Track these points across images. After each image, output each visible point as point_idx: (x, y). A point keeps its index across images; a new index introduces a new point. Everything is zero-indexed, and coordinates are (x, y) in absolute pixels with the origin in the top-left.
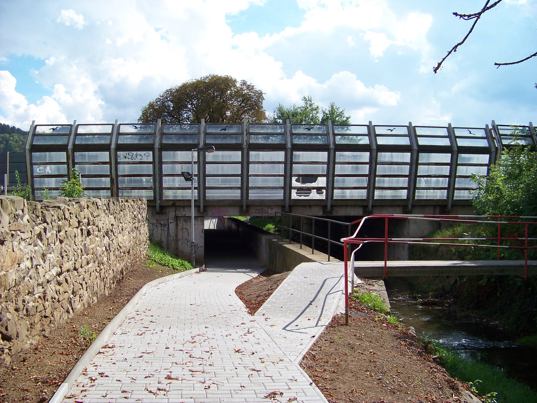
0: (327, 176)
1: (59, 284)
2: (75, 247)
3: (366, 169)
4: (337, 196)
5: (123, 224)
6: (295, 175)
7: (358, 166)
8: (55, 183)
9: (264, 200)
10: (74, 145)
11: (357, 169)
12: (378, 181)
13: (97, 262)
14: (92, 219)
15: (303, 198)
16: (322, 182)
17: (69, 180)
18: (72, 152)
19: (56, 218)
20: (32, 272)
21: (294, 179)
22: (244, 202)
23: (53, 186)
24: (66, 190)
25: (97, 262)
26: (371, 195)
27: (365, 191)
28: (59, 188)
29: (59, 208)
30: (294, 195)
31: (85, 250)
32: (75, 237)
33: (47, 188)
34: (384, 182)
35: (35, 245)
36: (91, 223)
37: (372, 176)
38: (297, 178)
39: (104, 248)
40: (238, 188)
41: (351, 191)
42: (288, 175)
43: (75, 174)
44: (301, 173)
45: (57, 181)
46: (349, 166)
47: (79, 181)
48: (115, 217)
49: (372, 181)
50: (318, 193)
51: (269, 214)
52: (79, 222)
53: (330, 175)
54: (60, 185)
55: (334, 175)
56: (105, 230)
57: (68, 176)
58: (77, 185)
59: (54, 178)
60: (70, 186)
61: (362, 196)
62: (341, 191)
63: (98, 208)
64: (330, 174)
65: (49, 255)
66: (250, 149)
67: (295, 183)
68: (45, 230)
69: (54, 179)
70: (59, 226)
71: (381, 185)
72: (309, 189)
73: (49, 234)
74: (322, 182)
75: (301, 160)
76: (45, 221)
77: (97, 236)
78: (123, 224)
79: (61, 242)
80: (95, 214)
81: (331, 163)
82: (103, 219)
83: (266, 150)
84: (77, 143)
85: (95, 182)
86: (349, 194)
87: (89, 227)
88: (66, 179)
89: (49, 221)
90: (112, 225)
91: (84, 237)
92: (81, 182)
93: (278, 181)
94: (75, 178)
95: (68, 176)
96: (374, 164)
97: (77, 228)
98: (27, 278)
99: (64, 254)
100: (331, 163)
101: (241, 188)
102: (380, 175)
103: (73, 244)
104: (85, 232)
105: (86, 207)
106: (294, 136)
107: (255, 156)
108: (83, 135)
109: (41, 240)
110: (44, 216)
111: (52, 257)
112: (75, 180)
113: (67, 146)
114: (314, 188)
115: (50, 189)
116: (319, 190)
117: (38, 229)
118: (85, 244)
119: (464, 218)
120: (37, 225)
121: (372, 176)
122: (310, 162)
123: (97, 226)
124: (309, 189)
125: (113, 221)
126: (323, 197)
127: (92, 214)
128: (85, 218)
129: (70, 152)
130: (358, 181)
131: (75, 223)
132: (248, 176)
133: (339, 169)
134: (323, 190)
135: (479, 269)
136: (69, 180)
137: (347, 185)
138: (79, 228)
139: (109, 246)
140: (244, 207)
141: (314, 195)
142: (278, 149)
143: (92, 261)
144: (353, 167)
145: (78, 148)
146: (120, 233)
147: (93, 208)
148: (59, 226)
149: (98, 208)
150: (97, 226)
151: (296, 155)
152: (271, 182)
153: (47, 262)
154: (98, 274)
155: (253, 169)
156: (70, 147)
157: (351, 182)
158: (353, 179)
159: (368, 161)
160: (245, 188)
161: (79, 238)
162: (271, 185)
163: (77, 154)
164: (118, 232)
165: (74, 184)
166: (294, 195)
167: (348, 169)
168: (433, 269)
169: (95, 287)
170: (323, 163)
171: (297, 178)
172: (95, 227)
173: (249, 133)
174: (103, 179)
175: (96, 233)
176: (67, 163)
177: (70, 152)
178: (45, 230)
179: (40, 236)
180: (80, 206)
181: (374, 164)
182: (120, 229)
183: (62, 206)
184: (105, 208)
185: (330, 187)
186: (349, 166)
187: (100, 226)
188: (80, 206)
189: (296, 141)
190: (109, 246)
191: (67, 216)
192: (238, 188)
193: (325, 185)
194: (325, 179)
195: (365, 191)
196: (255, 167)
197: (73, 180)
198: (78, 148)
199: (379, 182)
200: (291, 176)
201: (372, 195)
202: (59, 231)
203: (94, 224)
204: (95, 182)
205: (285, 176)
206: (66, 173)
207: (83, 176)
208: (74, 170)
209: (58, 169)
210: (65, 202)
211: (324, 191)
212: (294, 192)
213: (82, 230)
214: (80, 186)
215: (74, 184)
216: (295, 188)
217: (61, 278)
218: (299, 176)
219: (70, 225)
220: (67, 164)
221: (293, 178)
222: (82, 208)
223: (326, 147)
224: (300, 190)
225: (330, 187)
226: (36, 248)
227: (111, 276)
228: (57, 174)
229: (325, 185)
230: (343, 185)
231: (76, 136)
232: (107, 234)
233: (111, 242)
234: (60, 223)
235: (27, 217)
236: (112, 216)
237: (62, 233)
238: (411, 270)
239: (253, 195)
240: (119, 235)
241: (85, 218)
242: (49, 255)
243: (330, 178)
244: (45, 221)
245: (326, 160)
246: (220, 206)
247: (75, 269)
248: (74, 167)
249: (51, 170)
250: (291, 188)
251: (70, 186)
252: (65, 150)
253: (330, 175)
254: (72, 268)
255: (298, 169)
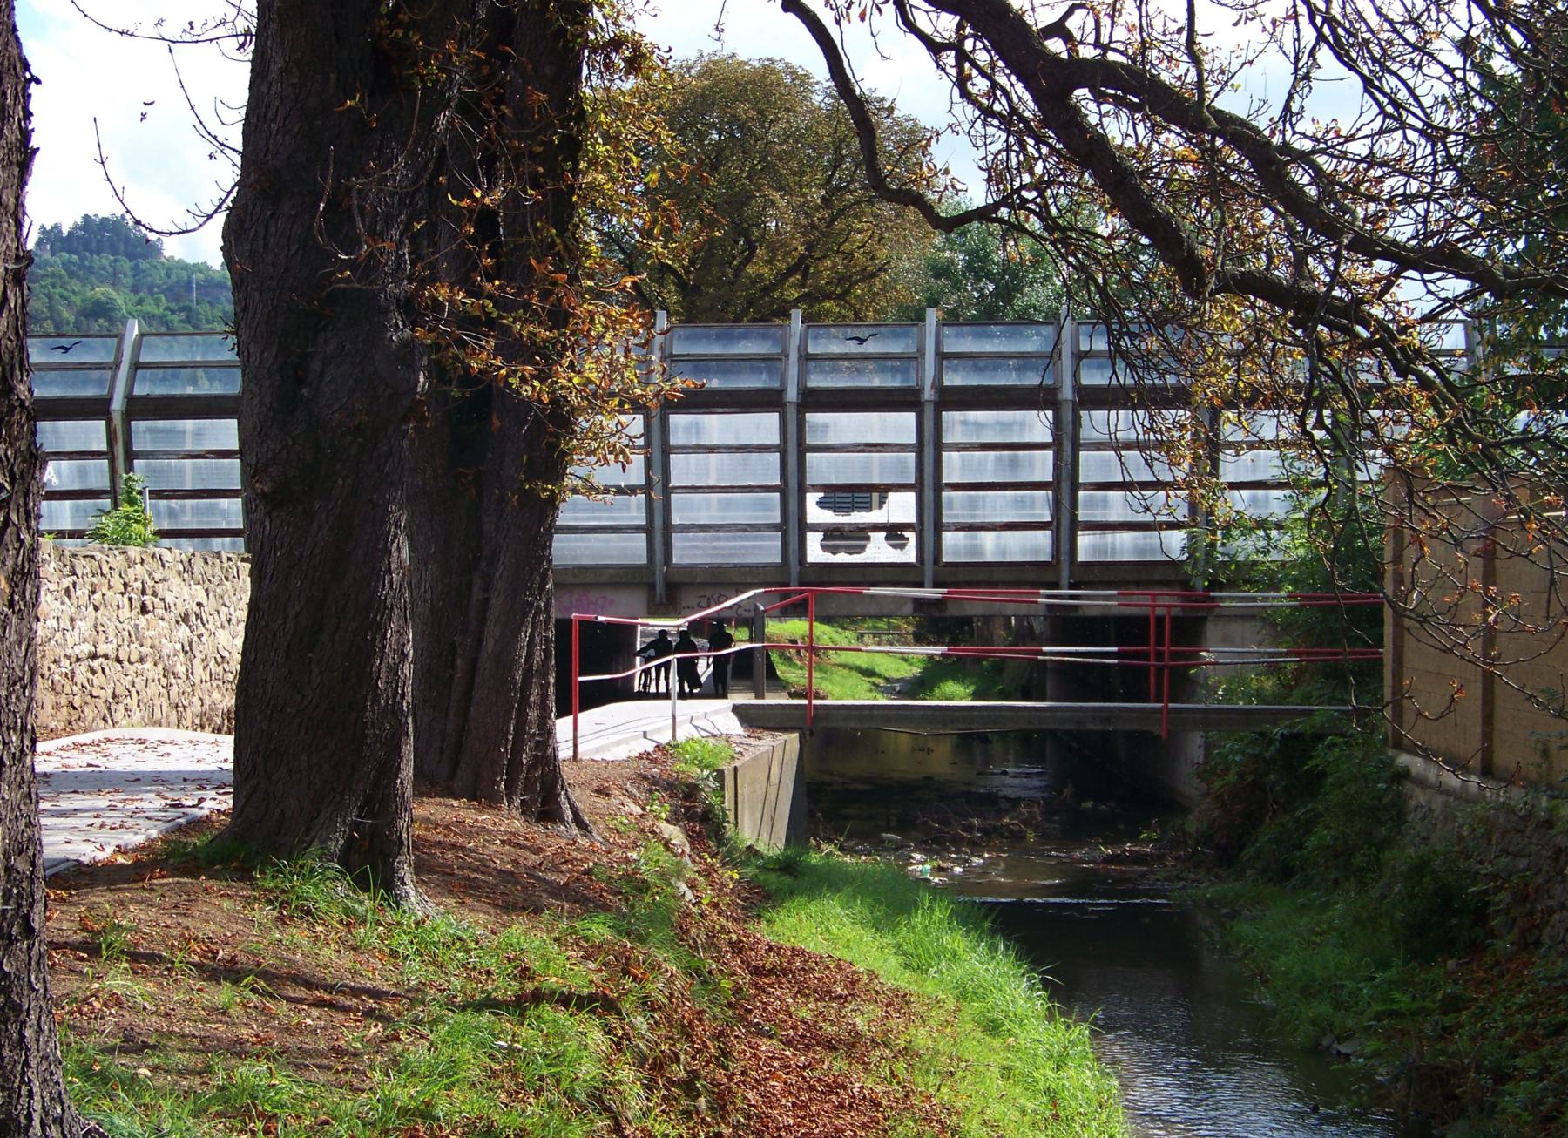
0: (917, 487)
1: (93, 672)
2: (118, 624)
3: (1042, 466)
4: (956, 553)
5: (232, 609)
6: (816, 488)
7: (1016, 456)
8: (73, 517)
9: (719, 567)
10: (131, 400)
11: (1014, 464)
12: (1085, 501)
13: (160, 667)
14: (150, 583)
15: (842, 558)
16: (901, 507)
17: (116, 506)
18: (123, 420)
19: (88, 571)
20: (59, 635)
21: (812, 499)
22: (658, 573)
23: (67, 525)
24: (106, 535)
25: (160, 667)
26: (1065, 547)
27: (1043, 538)
28: (84, 531)
29: (93, 557)
30: (815, 551)
31: (136, 636)
32: (118, 607)
33: (50, 532)
34: (1105, 504)
35: (63, 603)
36: (149, 591)
37: (1065, 486)
38: (822, 495)
39: (179, 647)
40: (637, 529)
41: (998, 538)
42: (792, 488)
43: (133, 490)
44: (834, 481)
45: (77, 511)
46: (986, 457)
47: (144, 511)
48: (207, 591)
49: (1066, 502)
50: (894, 546)
51: (740, 612)
52: (125, 585)
53: (929, 486)
54: (88, 523)
55: (939, 487)
56: (182, 611)
57: (112, 493)
58: (137, 522)
59: (68, 502)
60: (117, 524)
61: (1037, 552)
62: (966, 538)
63: (163, 566)
64: (926, 483)
65: (78, 622)
66: (670, 408)
67: (816, 513)
68: (74, 584)
69: (68, 504)
70: (92, 584)
71: (1098, 516)
72: (860, 534)
73: (79, 593)
74: (901, 507)
75: (831, 440)
76: (74, 574)
77: (163, 619)
78: (232, 609)
79: (96, 608)
80: (157, 576)
81: (929, 447)
82: (174, 588)
83: (721, 410)
84: (137, 391)
85: (190, 514)
86: (991, 546)
87: (145, 597)
88: (106, 503)
89: (79, 572)
90: (199, 604)
91: (134, 612)
92: (149, 513)
93: (765, 506)
94: (132, 502)
95: (112, 493)
96: (1067, 448)
97: (122, 594)
98: (53, 642)
99: (100, 629)
100: (929, 447)
101: (648, 529)
102: (1091, 484)
103: (114, 618)
104: (137, 605)
105: (138, 560)
106: (812, 364)
107: (687, 429)
108: (158, 368)
109: (69, 597)
110: (73, 567)
111: (84, 626)
112: (130, 509)
113: (108, 401)
114: (876, 528)
115: (61, 534)
116: (894, 532)
117: (67, 582)
118: (136, 626)
119: (982, 593)
120: (65, 576)
121: (1065, 486)
122: (858, 445)
123: (162, 599)
124: (860, 534)
125: (202, 597)
126: (909, 555)
127: (150, 575)
128: (136, 580)
129: (117, 420)
130: (1020, 503)
131: (117, 583)
132: (667, 491)
133: (954, 467)
134: (907, 534)
135: (1048, 714)
136: (116, 506)
137: (985, 516)
138: (126, 596)
139: (190, 644)
140: (660, 589)
141: (878, 551)
142: (727, 406)
143: (150, 659)
144: (999, 460)
145: (140, 408)
146: (223, 627)
147: (152, 564)
148: (92, 584)
149: (163, 566)
150: (162, 599)
151: (815, 427)
152: (743, 510)
153: (76, 630)
154: (164, 691)
155: (683, 469)
156: (117, 404)
157: (999, 506)
158: (1004, 497)
159: (1049, 439)
160: (659, 528)
161: (125, 613)
162: (704, 520)
163: (139, 426)
164: (219, 624)
165: (128, 518)
166: (815, 551)
167: (988, 466)
168: (930, 713)
169: (157, 711)
170: (902, 448)
171: (822, 495)
172: (156, 600)
173: (672, 355)
174: (224, 503)
175: (160, 612)
176: (110, 455)
177: (117, 420)
178: (74, 584)
179: (67, 591)
180: (128, 559)
181: (1067, 448)
182: (224, 619)
183: (98, 556)
184: (181, 568)
185: (930, 523)
186: (986, 457)
187: (169, 599)
188: (128, 559)
189: (817, 381)
190: (190, 644)
191: (106, 570)
192: (637, 529)
193: (911, 518)
194: (910, 498)
195: (1043, 538)
196: (688, 464)
197: (125, 508)
198: (140, 408)
199: (1091, 504)
200: (802, 490)
201: (1067, 547)
202: (94, 592)
203: (155, 594)
204: (190, 514)
205: (782, 490)
206: (106, 485)
207: (157, 494)
208: (130, 479)
209: (82, 473)
210: (101, 550)
211: (911, 536)
212: (814, 541)
213: (130, 599)
214: (145, 527)
215: (128, 518)
216: (815, 528)
217: (96, 664)
218: (825, 488)
219: (110, 587)
220: (109, 456)
221: (808, 495)
222: (130, 562)
223: (910, 398)
224: (833, 535)
225: (930, 523)
226: (64, 607)
227: (197, 708)
228: (76, 486)
229: (911, 518)
230: (973, 516)
231: (137, 369)
232: (185, 619)
233: (195, 639)
234: (94, 580)
235: (53, 565)
236: (199, 587)
237: (98, 596)
238: (876, 712)
239: (686, 551)
240: (220, 630)
241: (136, 580)
242: (78, 622)
243: (929, 495)
244: (74, 574)
245: (911, 438)
246: (587, 586)
247: (119, 661)
248: (129, 468)
249: (59, 474)
250: (804, 527)
251: (117, 524)
252: (103, 414)
253: (929, 486)
254: (113, 656)
255: (821, 468)
